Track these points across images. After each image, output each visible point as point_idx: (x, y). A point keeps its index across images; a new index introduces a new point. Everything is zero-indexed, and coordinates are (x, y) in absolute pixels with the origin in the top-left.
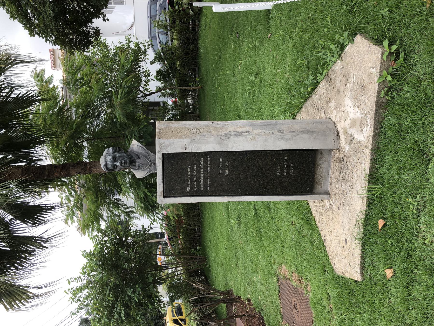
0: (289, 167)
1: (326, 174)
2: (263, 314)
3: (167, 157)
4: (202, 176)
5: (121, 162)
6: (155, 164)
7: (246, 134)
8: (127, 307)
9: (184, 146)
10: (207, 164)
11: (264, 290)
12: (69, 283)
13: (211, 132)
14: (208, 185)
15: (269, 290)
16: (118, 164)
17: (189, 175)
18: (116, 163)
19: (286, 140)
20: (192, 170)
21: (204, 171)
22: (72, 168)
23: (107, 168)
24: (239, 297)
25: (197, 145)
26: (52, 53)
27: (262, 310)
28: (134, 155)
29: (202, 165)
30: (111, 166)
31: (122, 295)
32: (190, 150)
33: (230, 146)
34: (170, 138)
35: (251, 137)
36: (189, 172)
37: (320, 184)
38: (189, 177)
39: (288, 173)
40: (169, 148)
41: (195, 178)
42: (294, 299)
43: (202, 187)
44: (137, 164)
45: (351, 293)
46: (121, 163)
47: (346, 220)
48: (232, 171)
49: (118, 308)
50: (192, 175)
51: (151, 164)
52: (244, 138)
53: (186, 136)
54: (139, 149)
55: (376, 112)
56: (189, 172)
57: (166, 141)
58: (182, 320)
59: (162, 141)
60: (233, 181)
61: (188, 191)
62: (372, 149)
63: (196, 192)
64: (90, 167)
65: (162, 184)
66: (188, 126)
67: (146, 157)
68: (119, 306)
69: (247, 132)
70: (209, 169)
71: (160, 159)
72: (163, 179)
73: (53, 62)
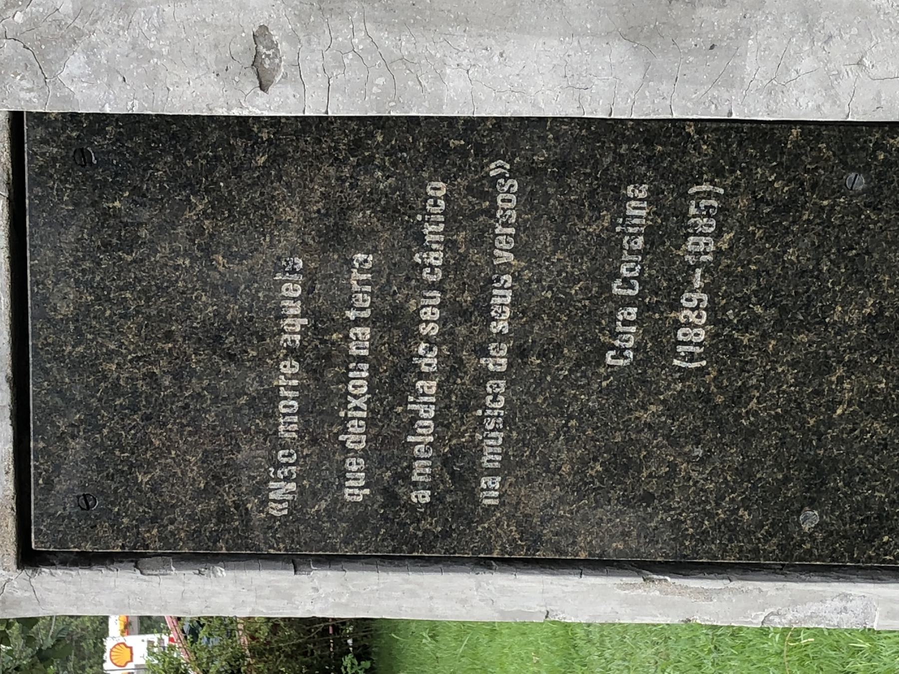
4: (429, 361)
9: (242, 45)
10: (483, 239)
14: (491, 457)
17: (291, 352)
21: (453, 313)
25: (385, 39)
29: (436, 258)
33: (753, 65)
38: (501, 326)
40: (75, 63)
41: (359, 382)
43: (421, 471)
48: (745, 326)
56: (294, 325)
60: (751, 433)
61: (275, 510)
63: (359, 518)
70: (502, 298)
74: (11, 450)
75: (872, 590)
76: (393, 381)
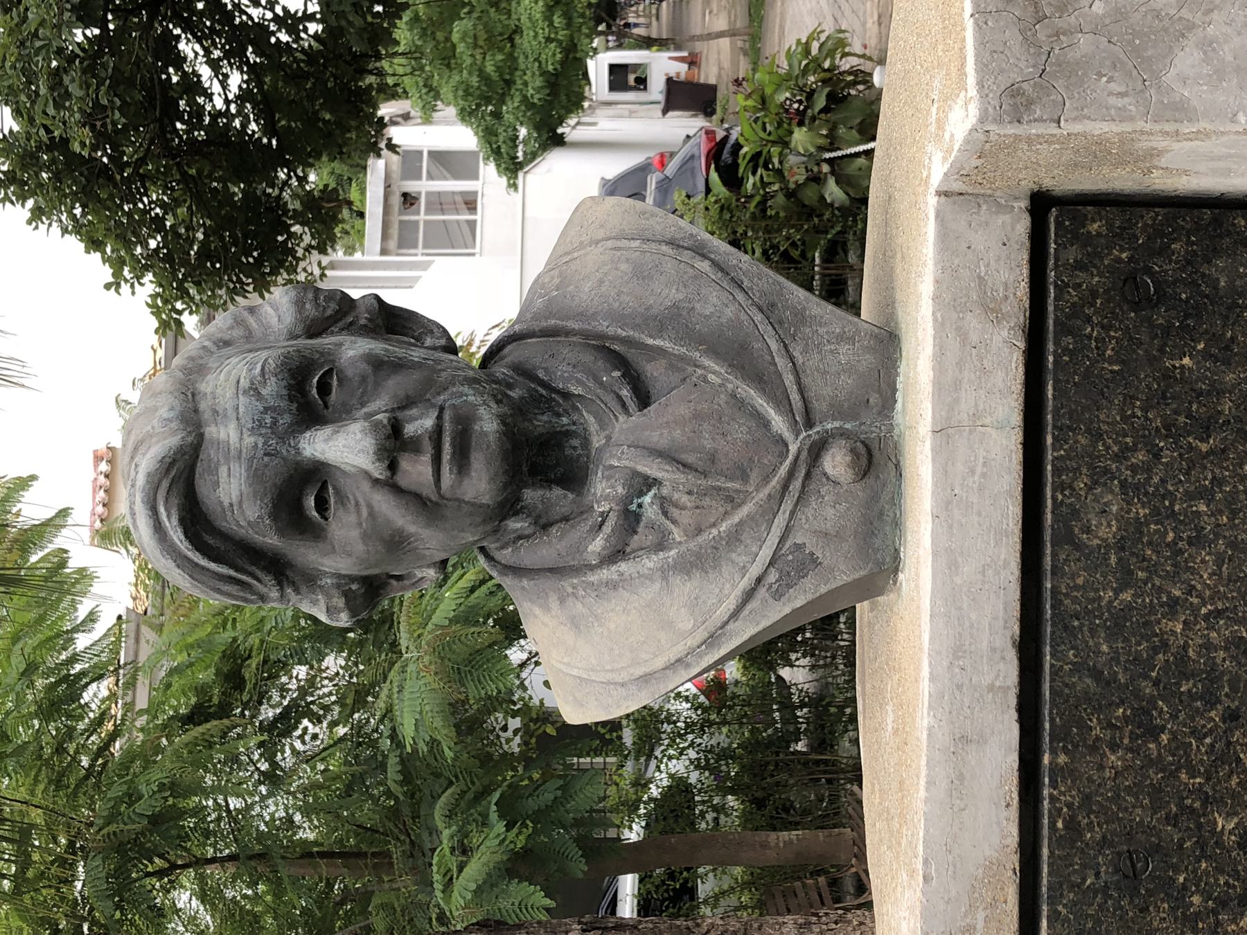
5: (396, 428)
6: (876, 460)
16: (344, 447)
26: (104, 467)
30: (256, 476)
44: (604, 491)
46: (394, 443)
51: (817, 450)
54: (641, 274)
65: (1011, 731)
67: (740, 356)
71: (992, 311)
73: (100, 509)
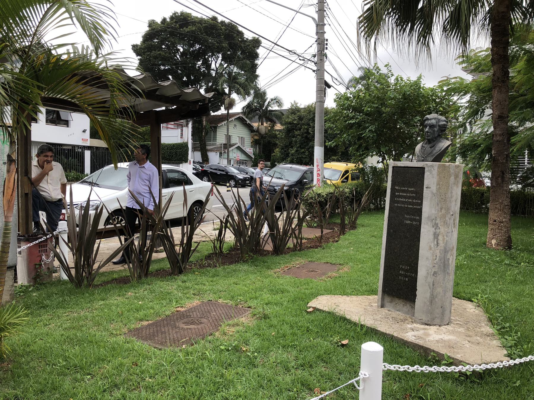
0: (406, 276)
1: (398, 309)
2: (319, 248)
3: (422, 170)
6: (423, 161)
7: (436, 243)
8: (359, 125)
9: (429, 186)
11: (338, 254)
12: (386, 66)
13: (441, 211)
15: (336, 257)
18: (428, 127)
19: (426, 277)
20: (412, 192)
22: (501, 67)
23: (425, 120)
24: (344, 234)
27: (324, 249)
28: (435, 143)
31: (371, 120)
32: (426, 192)
33: (426, 226)
34: (438, 175)
35: (432, 246)
36: (410, 189)
37: (391, 302)
39: (401, 275)
40: (429, 173)
41: (405, 194)
42: (319, 271)
45: (302, 299)
46: (427, 132)
47: (353, 310)
49: (359, 117)
50: (407, 192)
52: (432, 240)
53: (439, 189)
55: (422, 347)
56: (410, 189)
57: (435, 172)
58: (347, 178)
59: (436, 168)
62: (393, 336)
64: (500, 87)
66: (450, 192)
68: (360, 117)
69: (437, 243)
70: (411, 206)
72: (407, 167)
74: (111, 254)
75: (421, 342)
76: (405, 197)
